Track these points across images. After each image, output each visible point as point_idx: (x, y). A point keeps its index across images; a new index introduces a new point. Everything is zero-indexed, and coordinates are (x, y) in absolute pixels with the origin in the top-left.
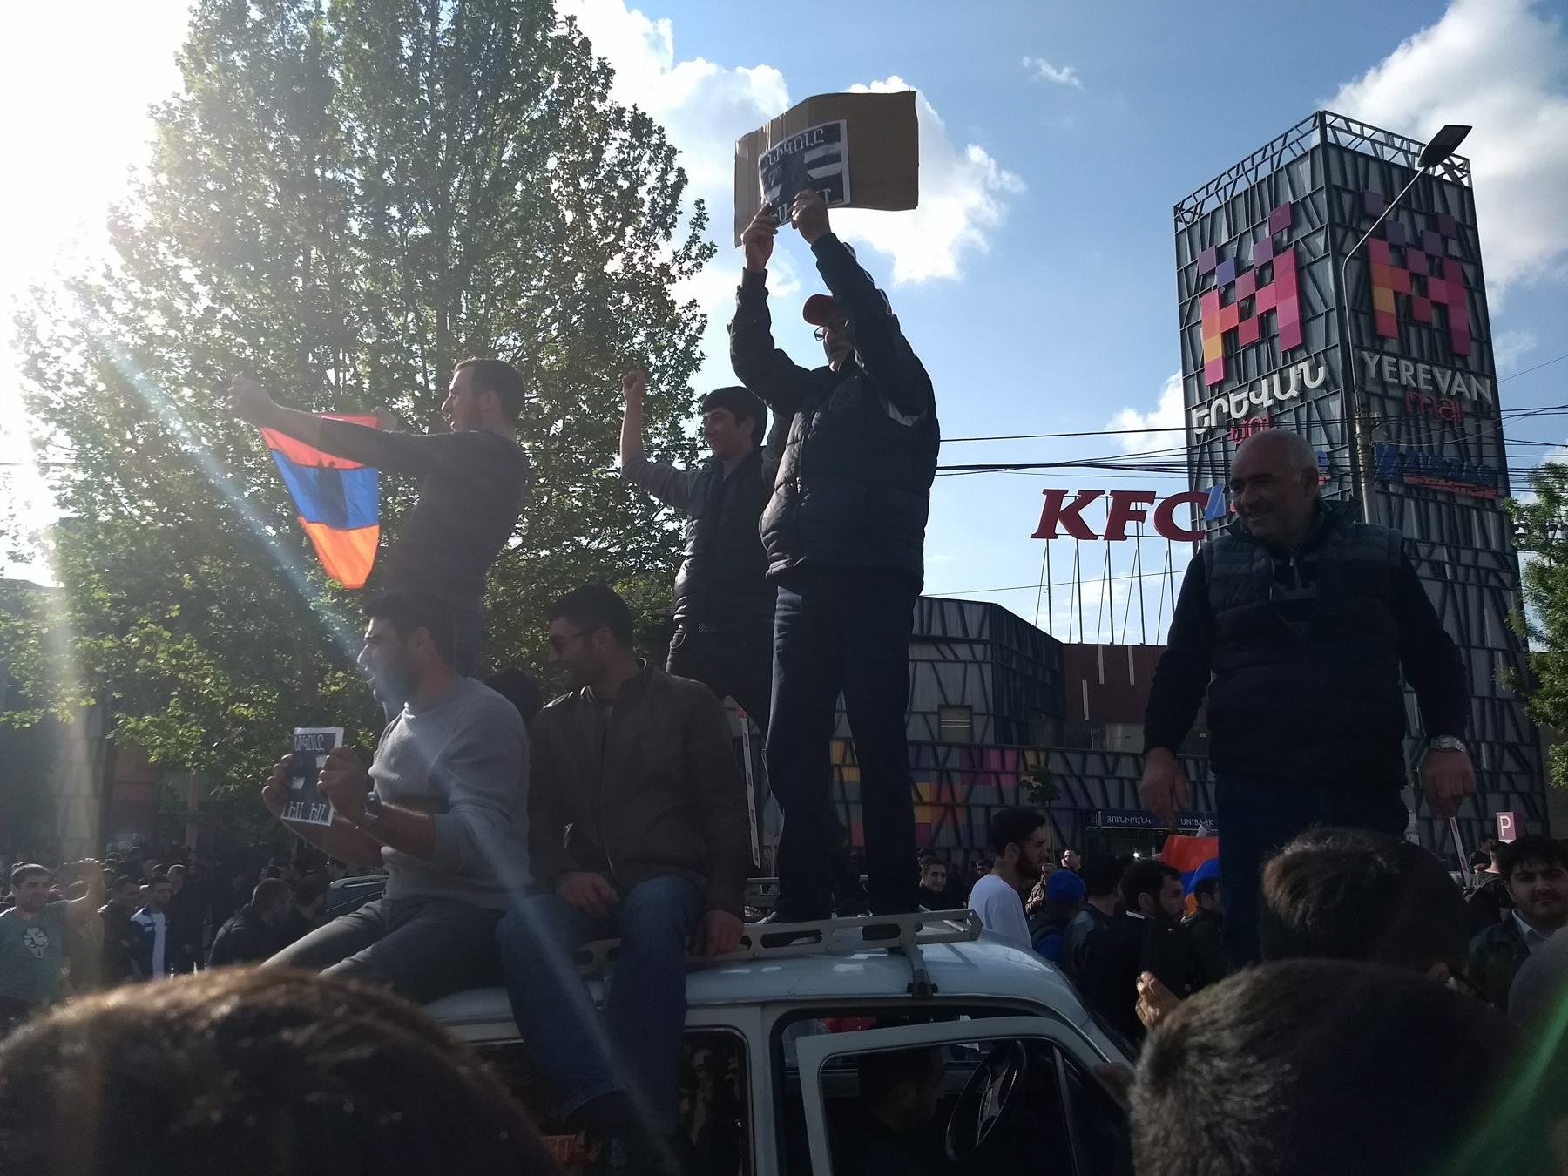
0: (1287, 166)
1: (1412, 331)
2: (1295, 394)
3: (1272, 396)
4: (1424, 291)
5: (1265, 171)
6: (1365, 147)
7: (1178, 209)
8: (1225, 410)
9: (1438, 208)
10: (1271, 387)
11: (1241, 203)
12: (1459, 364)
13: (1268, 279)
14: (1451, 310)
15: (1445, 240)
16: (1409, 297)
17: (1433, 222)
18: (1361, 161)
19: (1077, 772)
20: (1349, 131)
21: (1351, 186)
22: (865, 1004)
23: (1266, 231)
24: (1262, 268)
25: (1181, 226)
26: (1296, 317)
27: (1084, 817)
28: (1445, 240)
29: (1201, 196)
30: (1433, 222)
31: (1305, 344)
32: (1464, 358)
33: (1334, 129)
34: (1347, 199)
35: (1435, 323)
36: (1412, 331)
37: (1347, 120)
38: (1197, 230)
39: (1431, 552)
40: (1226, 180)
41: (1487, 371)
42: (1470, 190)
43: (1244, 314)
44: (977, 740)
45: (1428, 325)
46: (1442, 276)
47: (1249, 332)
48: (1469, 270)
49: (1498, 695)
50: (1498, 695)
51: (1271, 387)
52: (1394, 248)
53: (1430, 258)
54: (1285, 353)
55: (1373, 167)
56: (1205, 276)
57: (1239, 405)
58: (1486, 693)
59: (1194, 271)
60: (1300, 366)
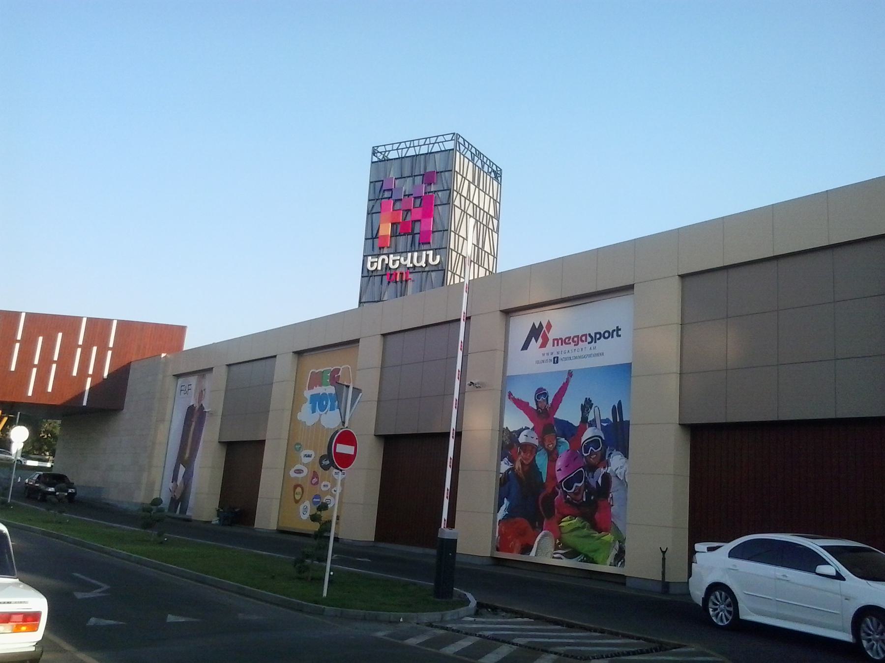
3: (412, 262)
5: (424, 150)
8: (386, 262)
10: (412, 257)
20: (464, 146)
25: (375, 159)
29: (389, 148)
51: (412, 257)
54: (554, 340)
57: (394, 261)
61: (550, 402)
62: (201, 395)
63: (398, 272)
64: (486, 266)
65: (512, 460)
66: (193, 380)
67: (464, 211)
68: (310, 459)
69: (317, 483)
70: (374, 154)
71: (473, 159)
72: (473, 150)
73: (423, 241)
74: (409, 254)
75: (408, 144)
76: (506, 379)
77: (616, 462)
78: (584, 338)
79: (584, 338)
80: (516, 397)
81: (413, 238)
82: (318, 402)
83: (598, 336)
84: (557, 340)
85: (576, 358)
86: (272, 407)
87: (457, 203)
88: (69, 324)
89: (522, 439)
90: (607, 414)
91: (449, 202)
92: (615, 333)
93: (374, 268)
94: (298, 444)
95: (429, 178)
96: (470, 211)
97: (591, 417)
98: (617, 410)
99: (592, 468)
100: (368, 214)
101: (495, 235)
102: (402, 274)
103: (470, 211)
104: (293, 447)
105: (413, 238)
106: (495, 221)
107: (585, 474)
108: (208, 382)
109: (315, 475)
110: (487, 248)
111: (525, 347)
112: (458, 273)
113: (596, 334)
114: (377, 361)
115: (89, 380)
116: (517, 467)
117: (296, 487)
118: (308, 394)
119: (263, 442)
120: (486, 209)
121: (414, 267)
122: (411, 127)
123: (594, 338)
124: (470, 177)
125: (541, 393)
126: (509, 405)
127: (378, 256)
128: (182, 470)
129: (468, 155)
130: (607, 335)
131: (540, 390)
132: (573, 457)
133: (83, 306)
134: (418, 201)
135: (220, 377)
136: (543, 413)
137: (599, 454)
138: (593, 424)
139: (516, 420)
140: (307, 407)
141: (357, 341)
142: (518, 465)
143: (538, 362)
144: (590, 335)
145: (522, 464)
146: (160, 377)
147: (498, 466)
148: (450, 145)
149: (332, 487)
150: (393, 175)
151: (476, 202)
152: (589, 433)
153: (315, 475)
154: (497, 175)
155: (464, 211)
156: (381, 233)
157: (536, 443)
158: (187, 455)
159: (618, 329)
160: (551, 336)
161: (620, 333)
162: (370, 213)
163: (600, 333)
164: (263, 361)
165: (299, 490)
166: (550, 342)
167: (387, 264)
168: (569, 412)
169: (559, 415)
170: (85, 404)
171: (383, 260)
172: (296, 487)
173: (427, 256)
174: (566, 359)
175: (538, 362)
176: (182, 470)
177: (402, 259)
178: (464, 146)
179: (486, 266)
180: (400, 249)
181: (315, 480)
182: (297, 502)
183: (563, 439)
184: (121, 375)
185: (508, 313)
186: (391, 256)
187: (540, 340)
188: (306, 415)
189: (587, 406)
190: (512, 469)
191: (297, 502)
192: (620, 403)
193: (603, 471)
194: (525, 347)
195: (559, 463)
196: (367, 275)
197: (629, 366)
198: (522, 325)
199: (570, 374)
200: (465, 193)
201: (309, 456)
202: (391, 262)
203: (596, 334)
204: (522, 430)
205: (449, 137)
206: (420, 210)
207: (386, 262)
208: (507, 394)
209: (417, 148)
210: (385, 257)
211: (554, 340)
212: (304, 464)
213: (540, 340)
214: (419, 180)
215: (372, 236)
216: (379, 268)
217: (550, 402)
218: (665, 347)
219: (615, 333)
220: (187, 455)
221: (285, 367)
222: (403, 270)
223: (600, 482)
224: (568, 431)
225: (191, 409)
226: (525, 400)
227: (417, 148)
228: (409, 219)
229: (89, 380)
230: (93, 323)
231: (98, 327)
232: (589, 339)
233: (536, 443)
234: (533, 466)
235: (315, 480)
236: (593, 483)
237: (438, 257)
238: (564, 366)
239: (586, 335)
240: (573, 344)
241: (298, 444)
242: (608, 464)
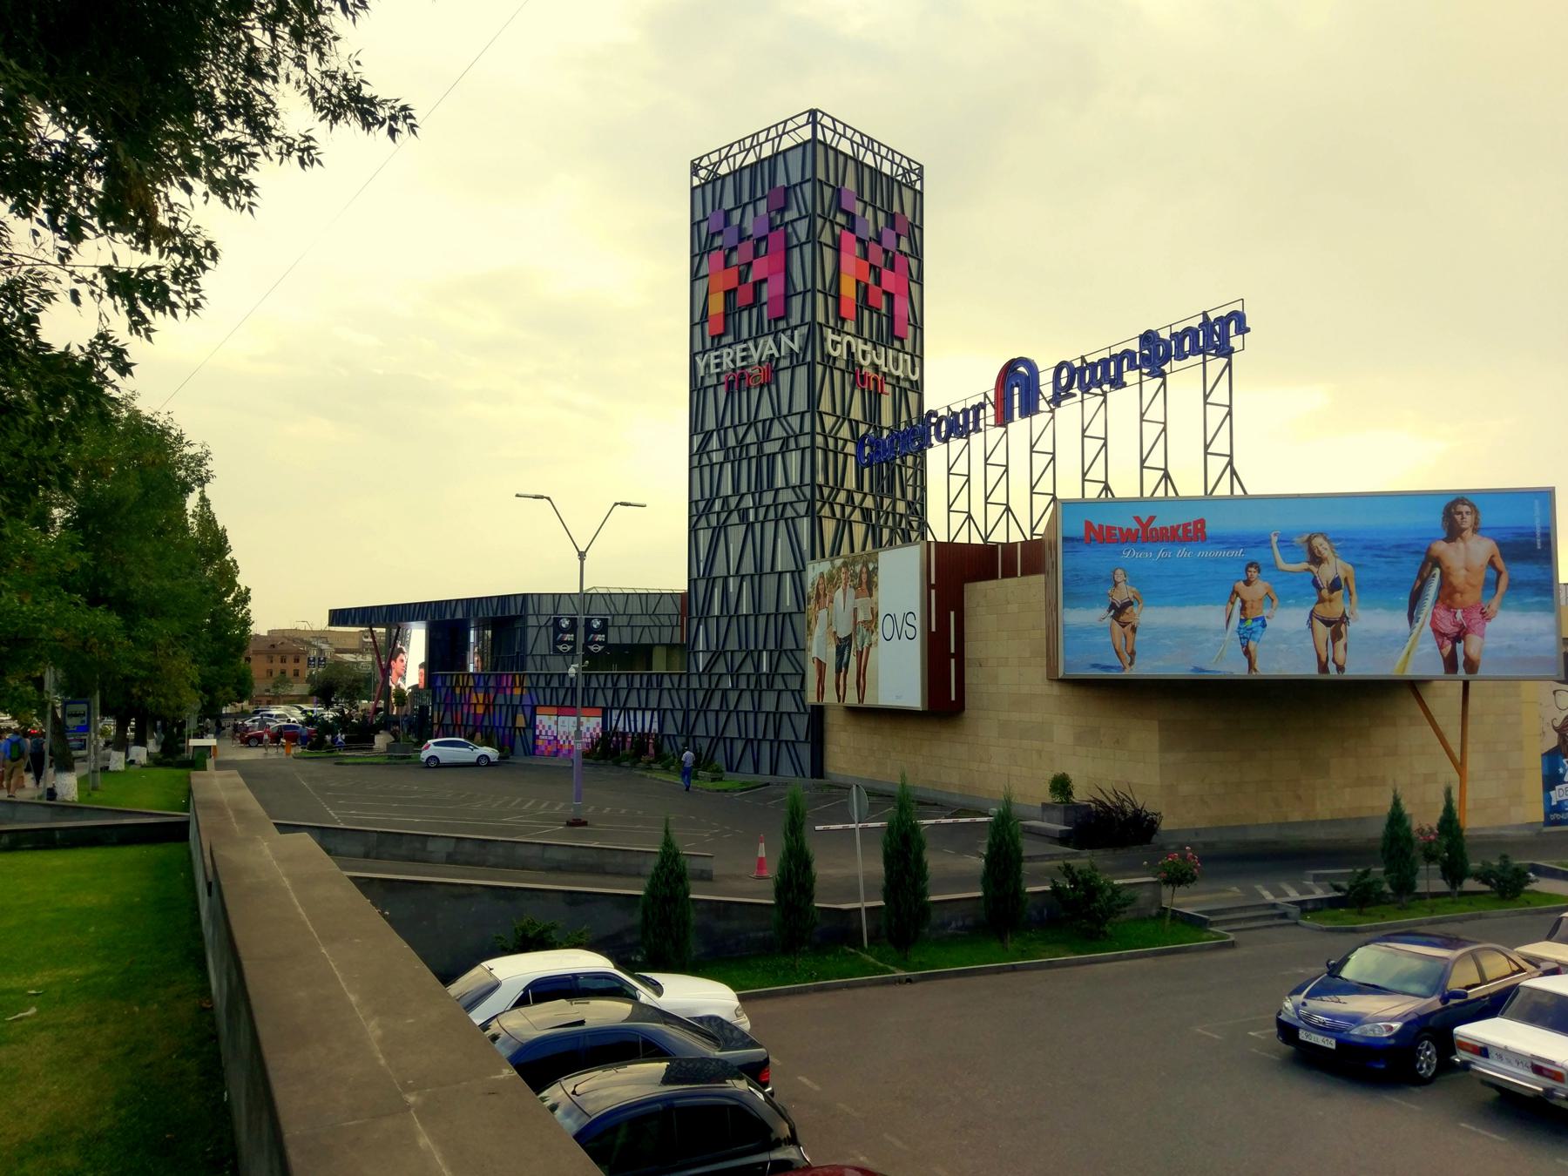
1: (866, 313)
4: (878, 282)
5: (767, 151)
6: (845, 146)
7: (695, 169)
9: (896, 208)
11: (747, 173)
12: (897, 344)
13: (763, 251)
14: (897, 298)
15: (898, 236)
16: (867, 286)
17: (892, 219)
18: (841, 159)
19: (846, 424)
21: (832, 182)
23: (762, 206)
24: (759, 240)
25: (696, 182)
26: (782, 290)
28: (898, 236)
30: (892, 219)
31: (786, 316)
32: (901, 340)
33: (823, 126)
34: (828, 192)
35: (884, 311)
36: (866, 313)
37: (834, 120)
38: (709, 188)
39: (863, 500)
40: (735, 149)
41: (917, 356)
42: (921, 194)
43: (742, 279)
44: (1147, 494)
45: (878, 310)
46: (893, 269)
47: (745, 296)
48: (913, 263)
49: (782, 610)
50: (782, 610)
52: (860, 240)
53: (886, 251)
55: (851, 164)
56: (713, 235)
58: (773, 610)
59: (704, 226)
148: (806, 134)
162: (695, 276)
205: (803, 120)
215: (699, 319)
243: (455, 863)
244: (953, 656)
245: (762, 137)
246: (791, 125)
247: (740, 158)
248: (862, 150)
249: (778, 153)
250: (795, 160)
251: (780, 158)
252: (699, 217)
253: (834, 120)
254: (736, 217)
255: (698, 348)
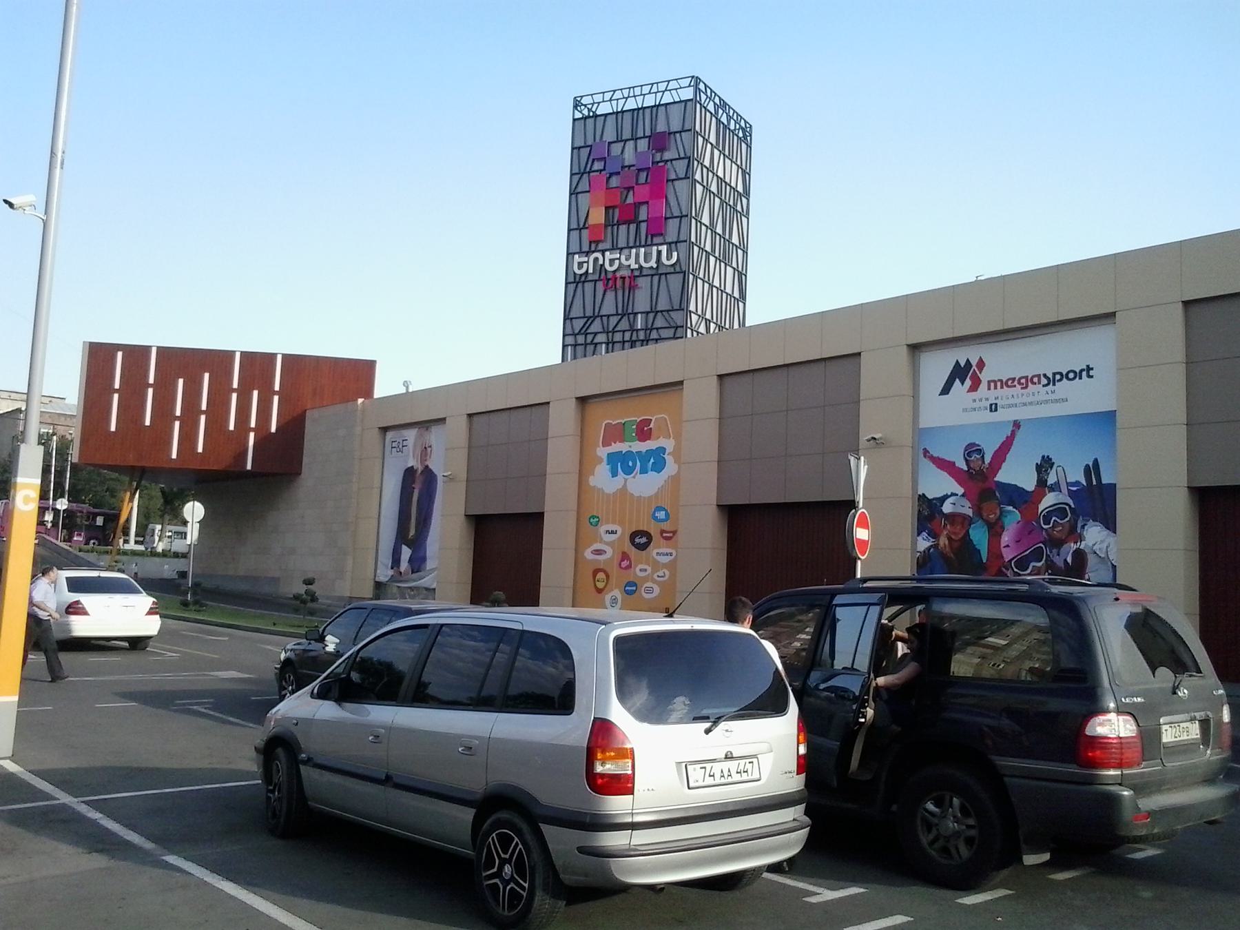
0: (667, 104)
2: (655, 266)
3: (637, 261)
5: (650, 101)
8: (601, 262)
10: (637, 255)
20: (706, 93)
22: (1172, 638)
25: (578, 115)
27: (781, 550)
29: (598, 98)
51: (637, 255)
54: (989, 382)
57: (612, 261)
60: (660, 248)
61: (988, 459)
62: (425, 451)
63: (618, 275)
64: (734, 265)
65: (934, 535)
66: (411, 435)
67: (706, 188)
68: (614, 537)
69: (629, 567)
70: (575, 107)
71: (716, 112)
72: (717, 100)
73: (656, 230)
74: (634, 251)
75: (626, 93)
76: (919, 433)
77: (1094, 535)
78: (1035, 380)
79: (1035, 380)
80: (935, 455)
81: (638, 229)
82: (621, 463)
83: (1058, 377)
84: (995, 382)
85: (1025, 404)
86: (549, 470)
87: (698, 177)
88: (217, 361)
89: (947, 508)
90: (1077, 476)
91: (688, 176)
92: (1084, 374)
93: (583, 270)
94: (593, 517)
95: (659, 141)
96: (714, 188)
97: (1051, 479)
98: (1093, 470)
99: (1057, 543)
100: (571, 194)
101: (744, 219)
102: (623, 278)
103: (714, 188)
104: (586, 521)
105: (638, 229)
106: (744, 200)
107: (1046, 551)
108: (435, 437)
109: (625, 556)
110: (735, 240)
111: (946, 390)
112: (701, 276)
113: (1054, 374)
114: (712, 409)
115: (252, 435)
116: (941, 543)
117: (596, 572)
118: (603, 452)
119: (537, 518)
120: (733, 184)
121: (641, 268)
122: (633, 68)
123: (1052, 380)
124: (713, 139)
125: (972, 450)
126: (928, 468)
127: (587, 254)
128: (406, 553)
129: (711, 107)
130: (1071, 376)
131: (972, 445)
132: (1027, 529)
133: (236, 335)
134: (643, 175)
135: (457, 429)
136: (979, 477)
137: (1067, 526)
138: (1055, 488)
139: (938, 484)
140: (603, 470)
141: (681, 383)
142: (943, 541)
143: (965, 410)
144: (1045, 375)
145: (950, 539)
146: (358, 430)
147: (914, 543)
148: (688, 94)
149: (653, 573)
150: (610, 135)
151: (720, 174)
152: (1049, 500)
153: (625, 556)
154: (746, 134)
155: (706, 188)
156: (591, 221)
157: (970, 512)
158: (412, 532)
159: (1089, 369)
160: (985, 376)
161: (1091, 373)
162: (574, 193)
163: (1061, 374)
164: (528, 410)
165: (601, 576)
166: (984, 386)
167: (602, 266)
168: (1018, 473)
169: (1002, 477)
170: (249, 467)
171: (596, 259)
172: (596, 572)
173: (659, 253)
174: (1010, 406)
175: (965, 410)
176: (406, 553)
177: (623, 257)
178: (706, 93)
179: (734, 265)
180: (622, 243)
181: (625, 563)
182: (599, 591)
183: (1011, 508)
184: (294, 427)
185: (915, 348)
186: (607, 253)
187: (968, 382)
188: (602, 479)
189: (1045, 465)
190: (935, 546)
191: (599, 591)
192: (1096, 461)
193: (1073, 547)
194: (946, 390)
195: (1006, 538)
196: (574, 282)
197: (1110, 416)
198: (938, 366)
199: (1017, 425)
200: (707, 163)
201: (612, 532)
202: (607, 263)
203: (1054, 374)
204: (946, 497)
205: (686, 82)
206: (647, 187)
207: (601, 262)
208: (921, 452)
209: (640, 99)
210: (599, 255)
211: (989, 382)
212: (606, 543)
213: (968, 382)
214: (643, 145)
215: (577, 226)
216: (591, 271)
217: (988, 459)
218: (1169, 396)
219: (1084, 374)
220: (412, 532)
221: (563, 419)
222: (626, 273)
223: (1069, 560)
224: (1014, 495)
225: (409, 473)
226: (951, 459)
227: (640, 99)
228: (630, 200)
229: (252, 435)
230: (249, 358)
231: (258, 365)
232: (1044, 381)
233: (970, 512)
234: (966, 541)
235: (625, 563)
236: (1059, 561)
237: (675, 254)
238: (1006, 415)
239: (1039, 376)
240: (1019, 387)
241: (593, 517)
242: (1080, 538)
243: (427, 589)
244: (275, 393)
245: (646, 89)
246: (673, 85)
247: (621, 102)
248: (720, 111)
249: (660, 105)
250: (676, 112)
251: (662, 109)
252: (579, 143)
253: (706, 86)
254: (616, 149)
255: (575, 248)
